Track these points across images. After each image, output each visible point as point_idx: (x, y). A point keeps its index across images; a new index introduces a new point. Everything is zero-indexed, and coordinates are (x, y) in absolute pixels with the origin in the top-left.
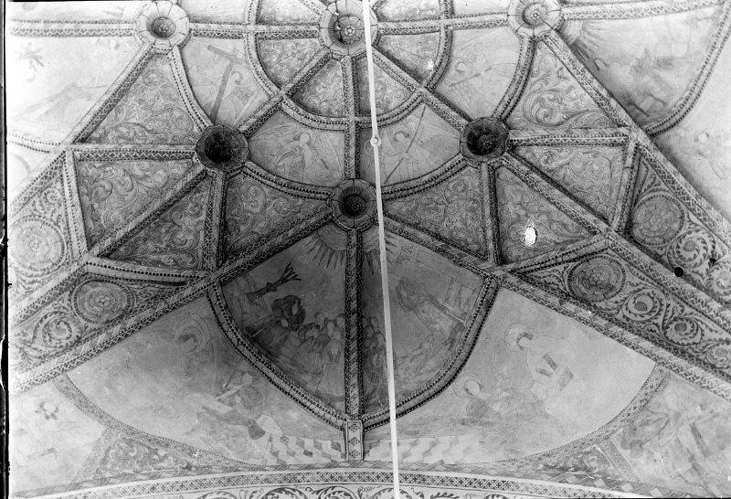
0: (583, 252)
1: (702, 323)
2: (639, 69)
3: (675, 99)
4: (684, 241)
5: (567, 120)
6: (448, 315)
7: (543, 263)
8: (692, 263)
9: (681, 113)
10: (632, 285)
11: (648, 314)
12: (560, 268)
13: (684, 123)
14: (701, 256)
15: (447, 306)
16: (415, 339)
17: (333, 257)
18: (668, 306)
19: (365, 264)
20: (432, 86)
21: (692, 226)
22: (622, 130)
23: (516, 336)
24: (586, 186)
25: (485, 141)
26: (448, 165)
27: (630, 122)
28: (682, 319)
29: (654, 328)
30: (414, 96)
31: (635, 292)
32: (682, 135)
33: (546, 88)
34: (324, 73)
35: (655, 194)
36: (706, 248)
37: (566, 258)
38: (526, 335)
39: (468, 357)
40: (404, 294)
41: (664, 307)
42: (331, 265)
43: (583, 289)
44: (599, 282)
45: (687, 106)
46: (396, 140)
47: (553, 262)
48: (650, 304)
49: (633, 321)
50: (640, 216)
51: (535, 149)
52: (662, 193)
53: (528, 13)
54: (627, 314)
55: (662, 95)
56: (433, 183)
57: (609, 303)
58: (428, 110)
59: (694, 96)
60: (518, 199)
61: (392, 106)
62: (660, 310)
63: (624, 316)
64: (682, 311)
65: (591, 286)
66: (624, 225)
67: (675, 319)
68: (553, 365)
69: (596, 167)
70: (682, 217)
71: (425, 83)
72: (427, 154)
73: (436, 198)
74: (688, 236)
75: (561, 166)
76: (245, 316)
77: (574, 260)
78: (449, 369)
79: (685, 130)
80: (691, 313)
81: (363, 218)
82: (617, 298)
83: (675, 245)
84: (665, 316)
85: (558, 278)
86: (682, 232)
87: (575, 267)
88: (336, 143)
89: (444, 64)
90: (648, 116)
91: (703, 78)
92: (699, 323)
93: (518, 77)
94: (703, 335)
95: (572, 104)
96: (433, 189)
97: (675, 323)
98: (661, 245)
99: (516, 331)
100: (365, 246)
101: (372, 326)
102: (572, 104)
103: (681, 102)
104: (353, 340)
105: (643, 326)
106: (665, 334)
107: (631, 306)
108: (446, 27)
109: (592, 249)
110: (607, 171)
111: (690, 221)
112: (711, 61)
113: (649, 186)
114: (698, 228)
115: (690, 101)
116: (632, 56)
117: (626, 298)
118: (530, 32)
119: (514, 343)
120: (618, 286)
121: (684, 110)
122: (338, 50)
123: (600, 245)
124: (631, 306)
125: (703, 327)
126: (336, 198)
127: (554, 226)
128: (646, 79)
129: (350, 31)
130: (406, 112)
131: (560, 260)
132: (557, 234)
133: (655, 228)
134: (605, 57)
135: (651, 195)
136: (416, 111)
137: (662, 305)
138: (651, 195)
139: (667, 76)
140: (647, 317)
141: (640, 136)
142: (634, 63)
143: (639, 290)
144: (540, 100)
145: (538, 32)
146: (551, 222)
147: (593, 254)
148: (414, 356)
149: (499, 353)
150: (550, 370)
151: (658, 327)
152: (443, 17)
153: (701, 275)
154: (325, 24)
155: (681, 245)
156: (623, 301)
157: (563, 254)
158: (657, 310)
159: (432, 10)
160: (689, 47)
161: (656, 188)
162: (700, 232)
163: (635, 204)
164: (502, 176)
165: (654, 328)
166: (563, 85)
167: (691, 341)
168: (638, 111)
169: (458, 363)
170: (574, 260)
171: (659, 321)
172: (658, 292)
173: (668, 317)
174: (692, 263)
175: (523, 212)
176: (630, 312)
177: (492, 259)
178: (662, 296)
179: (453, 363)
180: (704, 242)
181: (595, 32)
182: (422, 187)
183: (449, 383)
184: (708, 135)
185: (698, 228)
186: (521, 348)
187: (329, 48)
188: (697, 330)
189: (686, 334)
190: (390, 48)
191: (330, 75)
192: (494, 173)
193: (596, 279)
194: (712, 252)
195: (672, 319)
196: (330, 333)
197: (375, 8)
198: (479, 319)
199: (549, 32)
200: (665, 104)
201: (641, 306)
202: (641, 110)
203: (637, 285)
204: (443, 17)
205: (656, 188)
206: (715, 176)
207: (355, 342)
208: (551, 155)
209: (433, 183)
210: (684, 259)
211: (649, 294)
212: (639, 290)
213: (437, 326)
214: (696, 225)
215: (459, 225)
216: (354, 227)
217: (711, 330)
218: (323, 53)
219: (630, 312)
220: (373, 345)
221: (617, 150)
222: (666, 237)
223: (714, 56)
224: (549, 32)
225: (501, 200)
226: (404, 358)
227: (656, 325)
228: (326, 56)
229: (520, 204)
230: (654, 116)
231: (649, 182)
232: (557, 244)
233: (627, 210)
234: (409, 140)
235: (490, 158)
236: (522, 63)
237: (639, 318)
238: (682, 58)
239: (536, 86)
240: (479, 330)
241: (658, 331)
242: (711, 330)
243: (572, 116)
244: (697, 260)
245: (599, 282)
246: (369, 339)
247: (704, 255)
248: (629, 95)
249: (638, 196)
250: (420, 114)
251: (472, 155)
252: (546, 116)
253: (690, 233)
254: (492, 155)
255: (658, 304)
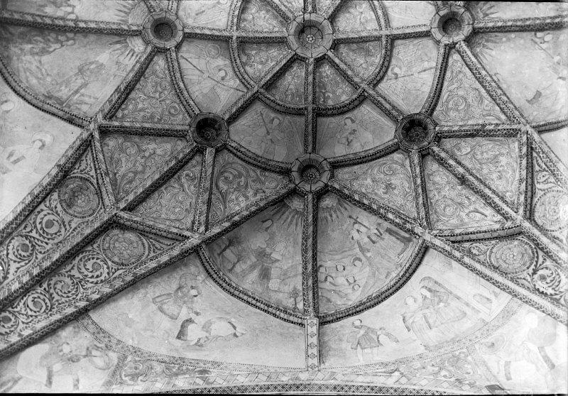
0: (103, 189)
1: (26, 264)
2: (262, 254)
3: (233, 278)
4: (101, 263)
5: (221, 192)
6: (70, 96)
7: (97, 159)
8: (82, 266)
9: (218, 279)
10: (70, 222)
11: (42, 228)
12: (93, 173)
13: (210, 283)
14: (86, 273)
15: (79, 95)
16: (55, 72)
17: (123, 14)
18: (47, 244)
19: (117, 38)
20: (260, 96)
21: (113, 270)
22: (202, 229)
23: (44, 139)
24: (163, 202)
25: (211, 133)
26: (191, 102)
27: (208, 234)
28: (32, 250)
29: (28, 229)
30: (252, 83)
31: (64, 223)
32: (199, 278)
33: (250, 180)
34: (276, 18)
35: (147, 248)
36: (93, 277)
37: (99, 176)
38: (43, 145)
39: (34, 106)
40: (93, 66)
41: (46, 240)
42: (117, 12)
43: (72, 186)
44: (76, 199)
45: (224, 285)
46: (220, 70)
47: (97, 167)
48: (53, 230)
49: (36, 216)
50: (130, 236)
51: (199, 168)
52: (147, 253)
53: (313, 170)
54: (45, 213)
55: (238, 269)
56: (178, 91)
57: (55, 203)
58: (241, 93)
59: (232, 290)
60: (159, 152)
61: (248, 68)
62: (44, 238)
63: (42, 210)
64: (41, 252)
65: (74, 192)
66: (122, 221)
67: (32, 245)
68: (15, 162)
69: (177, 210)
70: (123, 264)
71: (262, 90)
72: (205, 91)
73: (166, 92)
74: (105, 266)
75: (182, 186)
76: (437, 299)
77: (98, 183)
78: (24, 90)
79: (204, 281)
80: (37, 258)
81: (151, 35)
82: (59, 208)
83: (100, 256)
84: (38, 240)
85: (84, 170)
86: (110, 263)
87: (92, 184)
88: (217, 23)
89: (278, 107)
90: (219, 255)
91: (245, 298)
92: (27, 262)
93: (259, 159)
94: (15, 262)
95: (234, 197)
96: (173, 92)
97: (30, 245)
98: (101, 247)
99: (48, 139)
100: (132, 39)
101: (68, 40)
102: (234, 197)
103: (227, 279)
104: (52, 21)
105: (31, 222)
106: (21, 236)
107: (51, 217)
108: (306, 109)
109: (105, 196)
110: (173, 217)
111: (118, 270)
112: (258, 304)
113: (154, 245)
114: (111, 274)
115: (228, 287)
116: (274, 250)
117: (59, 215)
118: (295, 169)
119: (39, 137)
120: (71, 212)
121: (221, 282)
122: (293, 27)
123: (107, 202)
124: (51, 217)
125: (23, 264)
126: (168, 16)
127: (131, 175)
128: (254, 259)
129: (311, 39)
130: (241, 77)
131: (98, 172)
132: (124, 176)
133: (117, 245)
134: (274, 228)
135: (147, 246)
136: (242, 86)
137: (49, 239)
138: (147, 246)
139: (254, 275)
140: (39, 227)
141: (195, 240)
142: (268, 250)
143: (65, 226)
144: (240, 175)
145: (295, 174)
146: (136, 173)
147: (102, 198)
148: (41, 70)
149: (32, 127)
150: (12, 159)
151: (28, 232)
152: (315, 106)
153: (70, 271)
154: (313, 17)
155: (98, 261)
156: (57, 212)
157: (102, 174)
158: (45, 235)
159: (324, 101)
160: (276, 291)
161: (152, 249)
162: (107, 276)
163: (141, 234)
164: (179, 142)
165: (28, 229)
166: (250, 193)
167: (10, 251)
168: (223, 247)
169: (29, 97)
170: (98, 183)
171: (34, 234)
172: (61, 238)
173: (36, 241)
174: (82, 266)
175: (147, 154)
176: (45, 215)
177: (105, 122)
178: (56, 241)
179: (29, 93)
180: (97, 277)
181: (295, 221)
182: (175, 82)
183: (14, 90)
184: (195, 296)
185: (111, 274)
186: (34, 142)
187: (294, 20)
188: (20, 259)
189: (18, 250)
190: (295, 68)
191: (274, 22)
192: (180, 135)
193: (80, 197)
194: (88, 281)
195: (34, 244)
196: (63, 8)
197: (326, 57)
198: (61, 113)
199: (294, 183)
200: (230, 270)
201: (50, 224)
202: (224, 250)
203: (70, 225)
204: (315, 106)
205: (152, 249)
206: (157, 295)
207: (51, 22)
208: (193, 179)
209: (178, 91)
210: (86, 261)
211: (59, 231)
212: (65, 226)
213: (63, 88)
214: (113, 273)
215: (140, 106)
216: (144, 28)
217: (18, 268)
218: (290, 15)
219: (45, 215)
220: (52, 40)
221: (189, 225)
222: (108, 252)
223: (262, 306)
224: (294, 183)
225: (159, 139)
226: (40, 62)
227: (31, 231)
228: (288, 18)
229: (154, 153)
230: (219, 260)
231: (157, 245)
232: (115, 174)
233: (135, 225)
234: (219, 79)
235: (193, 133)
236: (271, 163)
237: (38, 221)
238: (268, 287)
239: (252, 174)
240: (54, 114)
241: (24, 231)
242: (18, 268)
243: (223, 197)
244: (83, 270)
245: (76, 199)
246: (57, 37)
247: (86, 276)
248: (239, 243)
249: (148, 236)
250: (240, 88)
251: (198, 120)
252: (226, 178)
253: (108, 268)
254: (195, 134)
255: (49, 237)
